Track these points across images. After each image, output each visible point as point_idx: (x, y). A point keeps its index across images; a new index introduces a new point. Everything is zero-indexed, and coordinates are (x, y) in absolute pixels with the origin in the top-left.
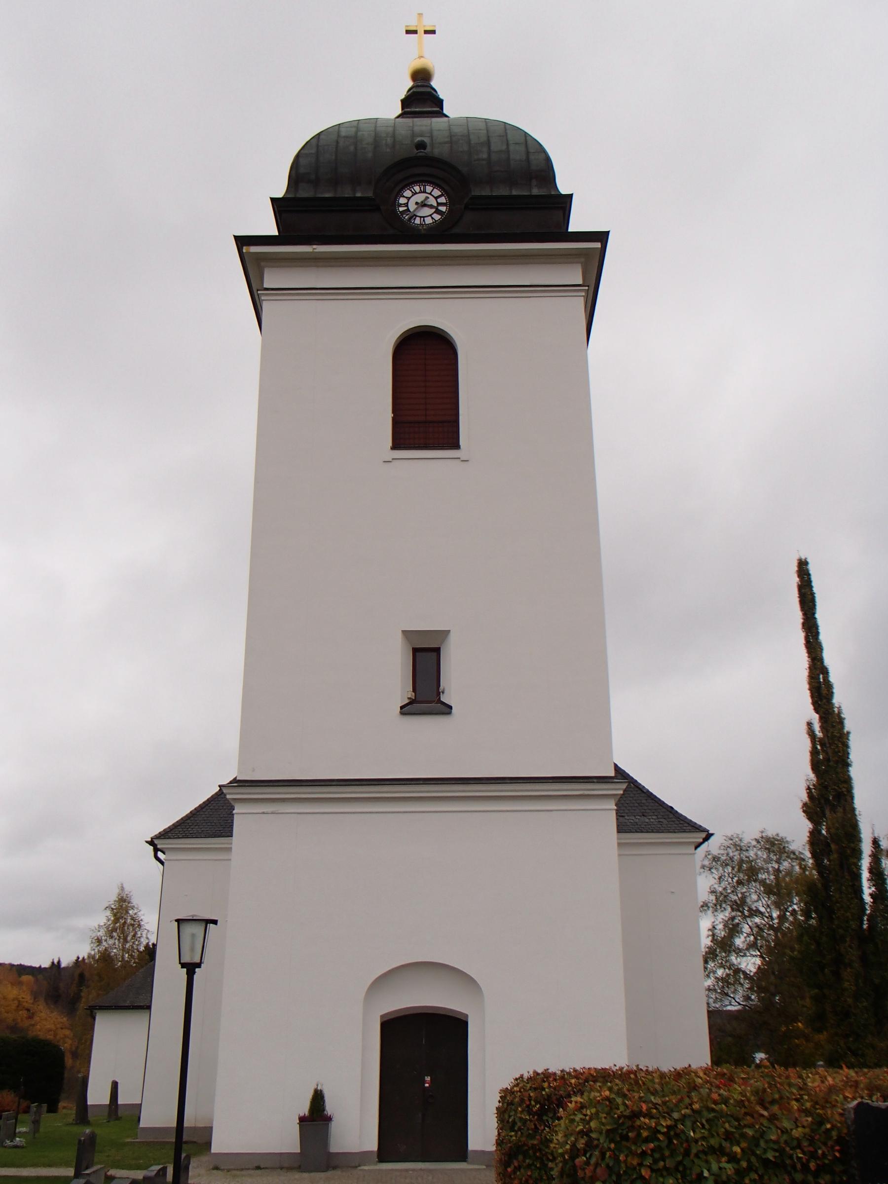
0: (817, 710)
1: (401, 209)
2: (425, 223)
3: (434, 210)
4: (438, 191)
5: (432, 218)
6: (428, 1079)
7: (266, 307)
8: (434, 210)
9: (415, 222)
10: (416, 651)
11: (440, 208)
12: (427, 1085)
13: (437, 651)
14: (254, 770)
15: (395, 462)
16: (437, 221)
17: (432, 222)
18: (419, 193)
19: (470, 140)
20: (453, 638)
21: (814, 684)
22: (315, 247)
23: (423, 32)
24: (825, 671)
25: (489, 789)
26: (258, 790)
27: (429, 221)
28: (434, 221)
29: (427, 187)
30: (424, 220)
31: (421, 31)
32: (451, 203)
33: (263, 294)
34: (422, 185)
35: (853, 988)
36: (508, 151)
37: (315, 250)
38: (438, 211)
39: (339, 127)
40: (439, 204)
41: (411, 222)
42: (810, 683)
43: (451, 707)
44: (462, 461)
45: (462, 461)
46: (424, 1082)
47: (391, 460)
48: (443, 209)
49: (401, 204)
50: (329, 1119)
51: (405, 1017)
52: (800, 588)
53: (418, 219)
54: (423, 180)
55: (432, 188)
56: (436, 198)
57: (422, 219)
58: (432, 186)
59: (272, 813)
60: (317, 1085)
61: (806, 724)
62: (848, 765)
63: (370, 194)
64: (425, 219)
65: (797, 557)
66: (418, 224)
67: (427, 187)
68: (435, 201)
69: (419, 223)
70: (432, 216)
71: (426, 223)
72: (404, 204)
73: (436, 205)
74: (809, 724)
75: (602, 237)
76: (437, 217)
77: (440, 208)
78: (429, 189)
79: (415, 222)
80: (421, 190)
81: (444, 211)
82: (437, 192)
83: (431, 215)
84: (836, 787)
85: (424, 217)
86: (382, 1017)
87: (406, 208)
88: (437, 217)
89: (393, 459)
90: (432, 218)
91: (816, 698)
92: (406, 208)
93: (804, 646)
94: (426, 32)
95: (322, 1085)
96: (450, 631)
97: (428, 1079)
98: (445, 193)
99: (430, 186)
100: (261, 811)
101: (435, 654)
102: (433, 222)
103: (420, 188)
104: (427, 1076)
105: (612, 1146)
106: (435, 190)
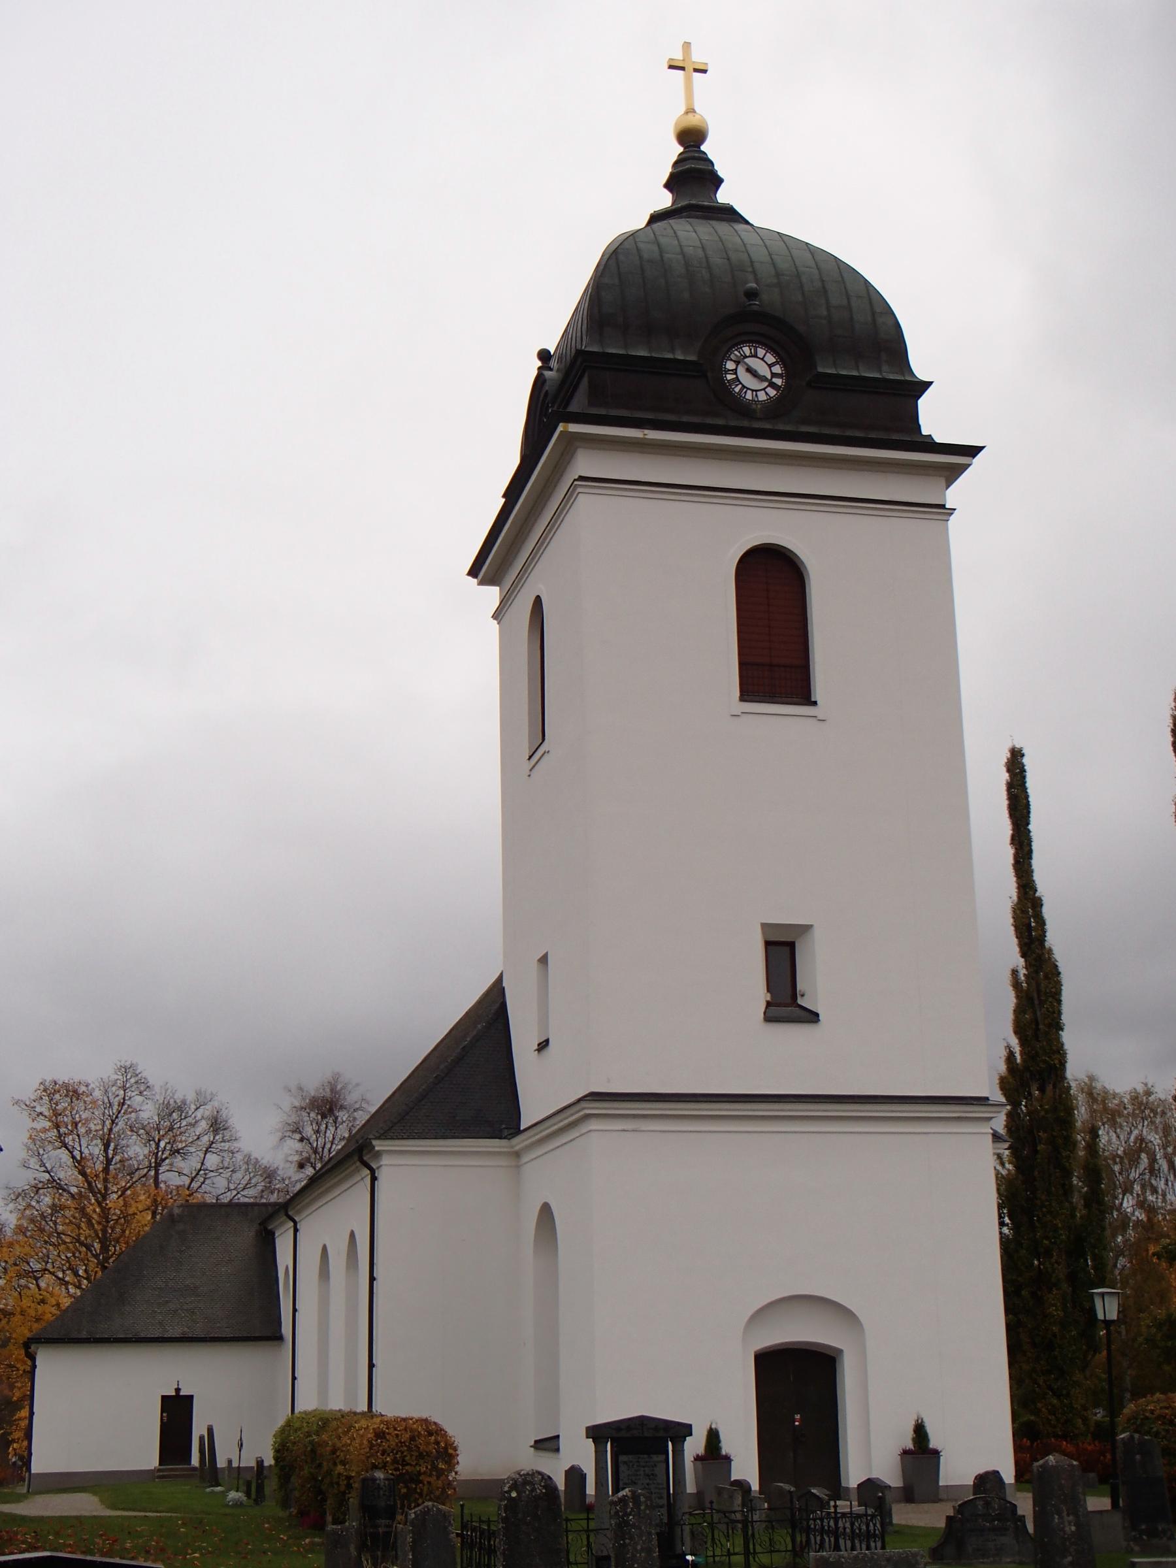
0: (1023, 955)
1: (729, 377)
2: (758, 399)
3: (766, 384)
4: (772, 357)
5: (767, 394)
6: (798, 1417)
7: (845, 302)
8: (766, 384)
9: (747, 397)
10: (768, 944)
11: (774, 380)
12: (797, 1423)
13: (791, 946)
14: (609, 1081)
15: (745, 717)
16: (772, 397)
17: (766, 399)
18: (749, 356)
19: (802, 286)
20: (818, 934)
21: (1024, 920)
22: (646, 431)
23: (692, 70)
24: (1037, 904)
25: (859, 1108)
26: (616, 1105)
27: (762, 396)
28: (768, 397)
29: (758, 349)
30: (756, 395)
31: (690, 68)
32: (788, 375)
33: (579, 485)
34: (752, 346)
35: (1061, 1314)
36: (849, 308)
37: (646, 437)
38: (772, 385)
39: (634, 238)
40: (774, 375)
41: (731, 387)
42: (1016, 918)
43: (817, 1015)
44: (819, 720)
45: (819, 720)
46: (801, 1420)
47: (739, 714)
48: (778, 381)
49: (729, 370)
50: (728, 1459)
51: (807, 1351)
52: (1010, 786)
53: (749, 392)
54: (757, 340)
55: (764, 352)
56: (770, 366)
57: (745, 390)
58: (764, 349)
59: (633, 1131)
60: (712, 1424)
61: (1010, 972)
62: (1059, 1027)
63: (692, 358)
64: (758, 393)
65: (1009, 745)
66: (750, 400)
67: (758, 349)
68: (757, 359)
69: (751, 398)
70: (766, 390)
71: (760, 399)
72: (732, 370)
73: (769, 377)
74: (1015, 972)
75: (955, 509)
76: (772, 392)
77: (774, 380)
78: (761, 352)
79: (747, 397)
80: (751, 353)
81: (780, 385)
82: (770, 359)
83: (764, 389)
84: (1047, 1059)
85: (756, 391)
86: (755, 1352)
87: (734, 376)
88: (772, 392)
89: (742, 713)
90: (767, 394)
91: (1026, 938)
92: (734, 376)
93: (1012, 867)
94: (696, 70)
95: (716, 1423)
96: (812, 926)
97: (798, 1417)
98: (781, 360)
99: (781, 368)
100: (620, 1128)
101: (787, 949)
102: (767, 400)
103: (751, 350)
104: (797, 1414)
105: (505, 1538)
106: (768, 354)
